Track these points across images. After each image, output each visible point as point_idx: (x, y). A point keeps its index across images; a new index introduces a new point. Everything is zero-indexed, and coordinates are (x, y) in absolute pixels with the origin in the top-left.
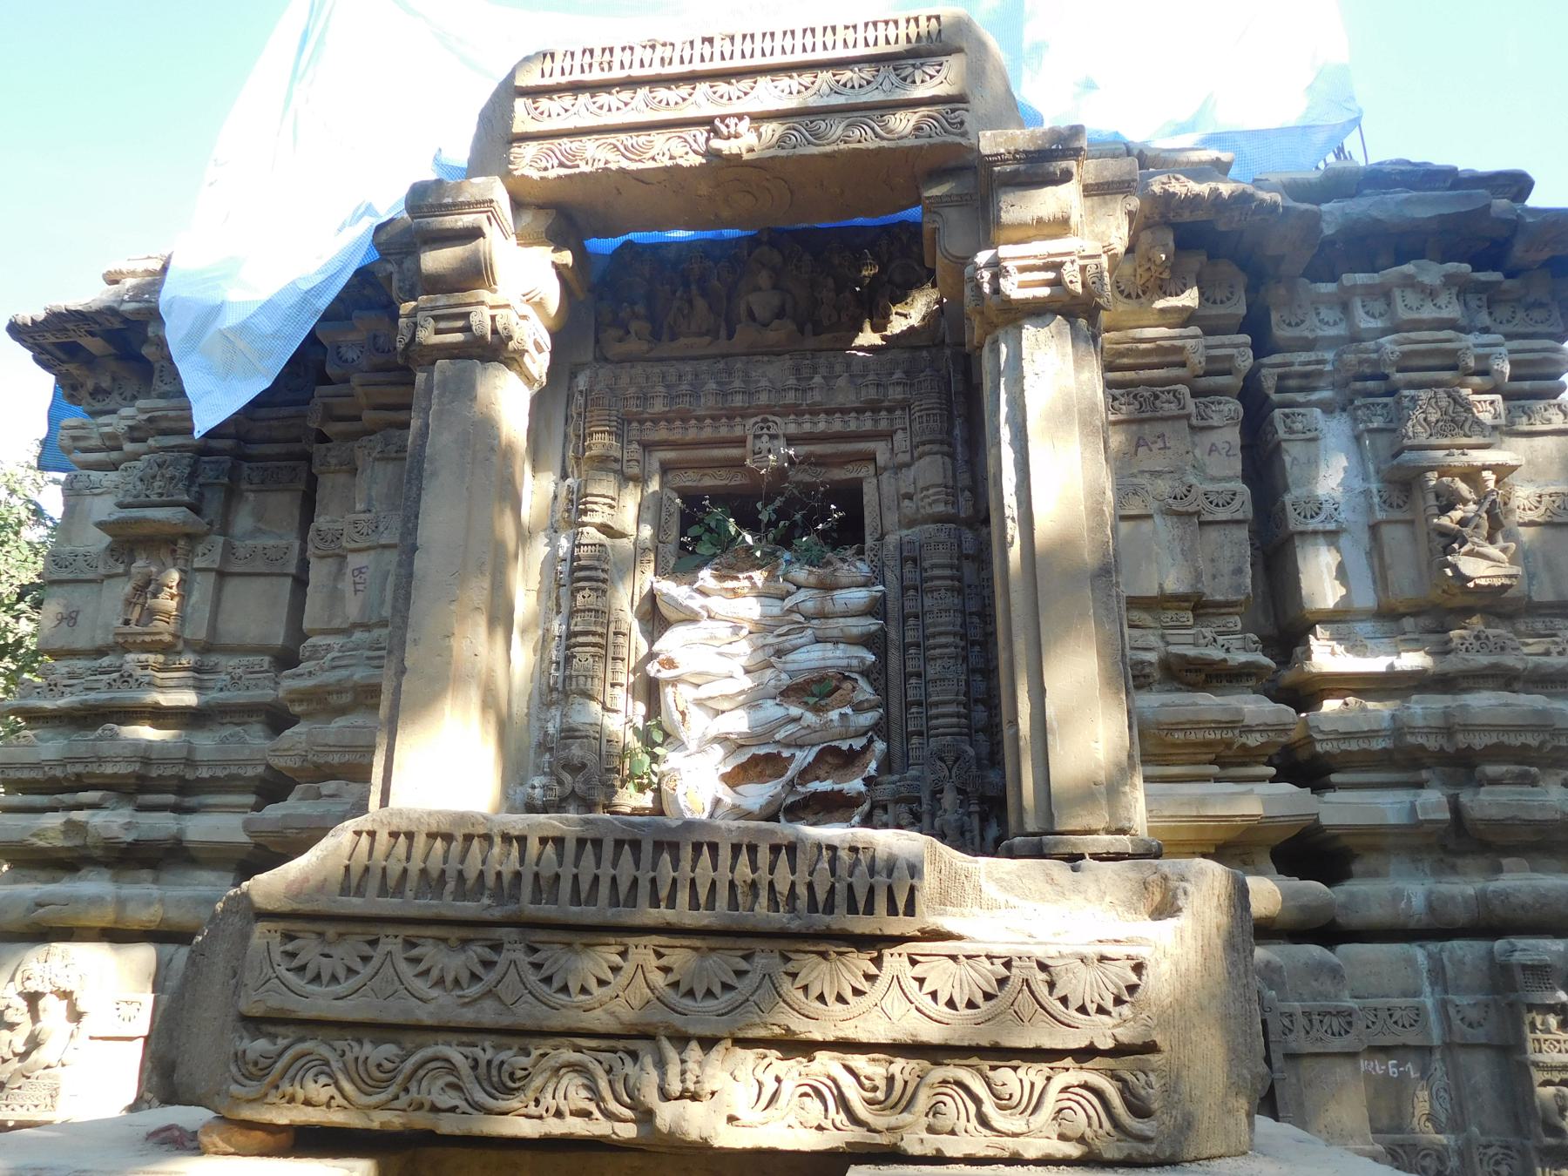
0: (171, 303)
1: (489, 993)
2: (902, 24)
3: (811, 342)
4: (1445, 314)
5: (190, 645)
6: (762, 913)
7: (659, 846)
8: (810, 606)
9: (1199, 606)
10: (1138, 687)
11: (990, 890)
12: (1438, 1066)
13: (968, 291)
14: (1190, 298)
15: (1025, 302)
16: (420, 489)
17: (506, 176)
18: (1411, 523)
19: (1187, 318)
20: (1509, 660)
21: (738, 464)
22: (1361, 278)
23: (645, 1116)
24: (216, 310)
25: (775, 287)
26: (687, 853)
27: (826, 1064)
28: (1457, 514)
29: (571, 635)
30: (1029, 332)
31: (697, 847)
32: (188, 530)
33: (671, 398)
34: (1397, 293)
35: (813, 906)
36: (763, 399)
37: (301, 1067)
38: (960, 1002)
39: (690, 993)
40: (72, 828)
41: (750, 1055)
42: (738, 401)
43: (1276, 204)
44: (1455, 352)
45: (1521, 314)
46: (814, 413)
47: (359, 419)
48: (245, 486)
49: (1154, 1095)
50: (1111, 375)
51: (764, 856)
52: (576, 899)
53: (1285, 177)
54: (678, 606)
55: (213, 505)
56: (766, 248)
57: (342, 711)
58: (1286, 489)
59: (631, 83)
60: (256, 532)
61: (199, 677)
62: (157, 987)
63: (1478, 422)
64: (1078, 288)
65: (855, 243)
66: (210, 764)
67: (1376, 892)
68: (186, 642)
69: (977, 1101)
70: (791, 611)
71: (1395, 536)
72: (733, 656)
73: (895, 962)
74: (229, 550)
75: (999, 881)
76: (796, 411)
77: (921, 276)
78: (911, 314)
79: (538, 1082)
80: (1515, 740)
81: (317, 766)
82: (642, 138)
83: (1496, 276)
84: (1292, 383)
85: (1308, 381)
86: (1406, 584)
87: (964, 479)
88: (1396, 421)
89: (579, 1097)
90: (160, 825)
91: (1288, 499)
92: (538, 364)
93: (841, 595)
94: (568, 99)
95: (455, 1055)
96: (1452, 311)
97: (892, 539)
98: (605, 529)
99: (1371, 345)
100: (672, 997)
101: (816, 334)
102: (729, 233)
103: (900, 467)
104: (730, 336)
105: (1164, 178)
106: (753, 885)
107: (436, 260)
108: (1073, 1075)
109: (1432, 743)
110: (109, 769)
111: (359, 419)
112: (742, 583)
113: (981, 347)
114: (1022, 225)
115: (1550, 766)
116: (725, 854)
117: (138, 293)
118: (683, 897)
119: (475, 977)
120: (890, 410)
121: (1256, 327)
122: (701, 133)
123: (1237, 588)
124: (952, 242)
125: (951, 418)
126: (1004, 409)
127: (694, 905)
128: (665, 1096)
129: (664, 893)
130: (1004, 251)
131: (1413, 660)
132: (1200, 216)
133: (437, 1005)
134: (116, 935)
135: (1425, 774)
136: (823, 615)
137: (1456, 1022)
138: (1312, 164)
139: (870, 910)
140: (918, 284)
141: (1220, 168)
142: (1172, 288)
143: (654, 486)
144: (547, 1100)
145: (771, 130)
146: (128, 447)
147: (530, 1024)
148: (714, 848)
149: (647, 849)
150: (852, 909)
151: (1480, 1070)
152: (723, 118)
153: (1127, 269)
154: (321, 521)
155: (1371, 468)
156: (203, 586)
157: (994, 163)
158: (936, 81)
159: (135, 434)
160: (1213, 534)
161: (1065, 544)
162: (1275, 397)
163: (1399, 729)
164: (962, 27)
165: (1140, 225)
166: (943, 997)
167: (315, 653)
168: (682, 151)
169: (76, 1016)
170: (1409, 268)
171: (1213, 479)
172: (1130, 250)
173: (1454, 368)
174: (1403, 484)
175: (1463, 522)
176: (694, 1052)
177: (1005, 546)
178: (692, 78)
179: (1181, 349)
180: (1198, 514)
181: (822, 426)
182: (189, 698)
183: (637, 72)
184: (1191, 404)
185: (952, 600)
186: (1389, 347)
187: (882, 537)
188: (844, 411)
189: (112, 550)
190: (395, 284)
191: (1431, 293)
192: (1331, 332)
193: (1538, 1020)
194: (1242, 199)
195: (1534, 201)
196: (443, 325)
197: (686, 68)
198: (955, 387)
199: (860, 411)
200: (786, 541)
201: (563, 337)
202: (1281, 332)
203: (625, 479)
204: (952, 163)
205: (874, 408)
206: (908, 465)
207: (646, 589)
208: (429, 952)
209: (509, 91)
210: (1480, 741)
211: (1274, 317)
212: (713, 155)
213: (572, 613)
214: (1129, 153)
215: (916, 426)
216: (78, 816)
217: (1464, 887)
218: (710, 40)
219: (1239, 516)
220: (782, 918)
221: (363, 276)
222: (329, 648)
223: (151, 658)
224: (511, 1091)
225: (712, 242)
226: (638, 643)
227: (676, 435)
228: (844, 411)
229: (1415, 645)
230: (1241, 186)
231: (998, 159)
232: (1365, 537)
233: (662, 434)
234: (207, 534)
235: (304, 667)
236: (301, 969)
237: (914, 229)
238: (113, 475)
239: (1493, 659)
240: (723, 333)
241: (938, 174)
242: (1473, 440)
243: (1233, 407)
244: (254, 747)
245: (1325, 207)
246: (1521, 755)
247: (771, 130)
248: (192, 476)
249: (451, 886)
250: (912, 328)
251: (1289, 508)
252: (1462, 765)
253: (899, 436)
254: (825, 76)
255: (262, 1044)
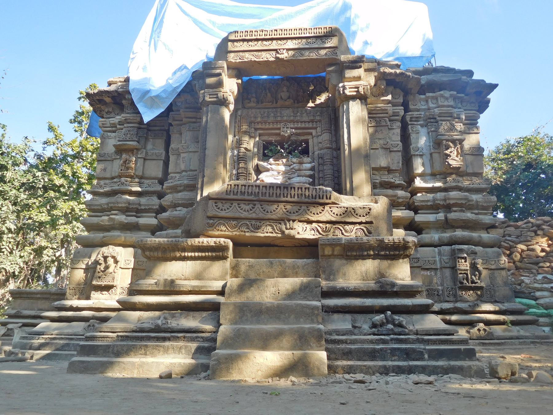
0: (133, 89)
1: (254, 212)
2: (323, 29)
3: (296, 105)
4: (450, 104)
5: (137, 177)
6: (303, 199)
7: (284, 188)
8: (297, 168)
9: (389, 170)
10: (374, 189)
11: (343, 200)
12: (439, 272)
13: (337, 93)
14: (389, 97)
15: (350, 96)
16: (206, 135)
17: (227, 61)
18: (440, 153)
19: (389, 102)
20: (460, 184)
21: (279, 134)
22: (431, 94)
23: (283, 232)
24: (148, 92)
25: (287, 91)
26: (289, 189)
27: (314, 225)
28: (449, 150)
29: (238, 173)
30: (351, 103)
31: (291, 188)
32: (137, 147)
33: (262, 118)
34: (439, 98)
35: (312, 198)
36: (285, 118)
37: (220, 224)
38: (339, 215)
39: (290, 213)
40: (111, 219)
41: (301, 223)
42: (279, 119)
43: (410, 76)
44: (451, 113)
45: (469, 105)
46: (298, 122)
47: (182, 121)
48: (150, 137)
49: (372, 230)
50: (370, 115)
51: (303, 189)
52: (269, 196)
53: (414, 69)
54: (264, 167)
55: (142, 141)
56: (286, 81)
57: (180, 191)
58: (411, 144)
59: (257, 40)
60: (154, 149)
61: (140, 184)
62: (135, 257)
63: (456, 129)
64: (363, 93)
65: (308, 81)
66: (145, 205)
67: (426, 237)
68: (137, 176)
69: (341, 231)
70: (292, 169)
71: (436, 156)
72: (278, 179)
73: (327, 208)
74: (147, 153)
75: (345, 199)
76: (293, 122)
77: (326, 90)
78: (322, 99)
79: (263, 227)
80: (459, 202)
81: (175, 204)
82: (260, 53)
83: (463, 95)
84: (414, 119)
85: (417, 119)
86: (438, 167)
87: (334, 139)
88: (438, 128)
89: (271, 230)
90: (133, 219)
91: (411, 147)
92: (232, 107)
93: (304, 165)
94: (241, 43)
95: (248, 223)
96: (452, 103)
97: (316, 153)
98: (246, 149)
99: (432, 111)
100: (287, 213)
101: (298, 103)
102: (276, 77)
103: (318, 136)
104: (276, 103)
105: (383, 68)
106: (302, 194)
107: (210, 81)
108: (358, 227)
109: (441, 203)
110: (120, 205)
111: (182, 121)
112: (280, 162)
113: (339, 107)
114: (350, 78)
115: (469, 209)
116: (296, 189)
117: (122, 87)
118: (289, 196)
119: (251, 210)
120: (316, 122)
121: (406, 106)
122: (274, 53)
123: (398, 167)
124: (333, 81)
125: (331, 124)
126: (345, 120)
127: (291, 197)
128: (287, 229)
129: (285, 195)
130: (346, 84)
131: (438, 184)
132: (392, 77)
133: (245, 214)
134: (124, 246)
135: (440, 210)
136: (300, 170)
137: (443, 262)
138: (419, 66)
139: (323, 198)
140: (323, 92)
141: (398, 66)
142: (385, 95)
143: (257, 139)
144: (265, 230)
145: (291, 53)
146: (118, 126)
147: (262, 217)
148: (294, 188)
149: (282, 188)
150: (320, 198)
151: (447, 272)
152: (279, 49)
153: (374, 90)
154: (172, 146)
155: (431, 140)
156: (140, 161)
157: (344, 63)
158: (331, 42)
159: (120, 123)
160: (393, 154)
161: (358, 150)
162: (409, 123)
163: (434, 200)
164: (337, 30)
165: (377, 79)
166: (336, 214)
167: (172, 177)
168: (270, 57)
169: (116, 262)
170: (442, 92)
171: (393, 141)
172: (375, 85)
173: (451, 117)
174: (439, 144)
175: (451, 152)
176: (291, 222)
177: (344, 151)
178: (272, 39)
179: (387, 110)
180: (389, 148)
181: (299, 125)
182: (139, 189)
183: (259, 37)
184: (389, 123)
185: (331, 167)
186: (436, 111)
187: (314, 153)
188: (305, 122)
189: (116, 152)
190: (197, 87)
191: (447, 99)
192: (424, 107)
193: (460, 261)
194: (402, 74)
195: (475, 77)
196: (211, 96)
197: (271, 37)
198: (333, 116)
199: (309, 122)
200: (290, 153)
201: (236, 100)
202: (411, 107)
203: (251, 137)
204: (334, 62)
205: (312, 121)
206: (320, 135)
207: (256, 164)
208: (242, 206)
209: (226, 41)
210: (452, 202)
211: (410, 103)
212: (277, 58)
213: (238, 168)
214: (376, 62)
215: (323, 126)
216: (111, 216)
217: (447, 235)
218: (277, 30)
219: (399, 150)
220: (307, 200)
221: (189, 83)
222: (176, 177)
223: (128, 179)
224: (258, 229)
225: (271, 79)
226: (254, 177)
227: (263, 127)
228: (305, 122)
229: (439, 181)
230: (402, 71)
231: (345, 62)
232: (429, 156)
233: (260, 126)
234: (142, 148)
235: (169, 181)
236: (219, 208)
237: (323, 79)
238: (114, 134)
239: (456, 184)
240: (275, 102)
241: (330, 65)
242: (455, 134)
243: (399, 124)
244: (154, 201)
245: (422, 77)
246: (460, 205)
247: (291, 53)
248: (137, 134)
249: (246, 194)
250: (322, 103)
251: (411, 149)
252: (448, 208)
253: (319, 128)
254: (304, 40)
255: (212, 221)
